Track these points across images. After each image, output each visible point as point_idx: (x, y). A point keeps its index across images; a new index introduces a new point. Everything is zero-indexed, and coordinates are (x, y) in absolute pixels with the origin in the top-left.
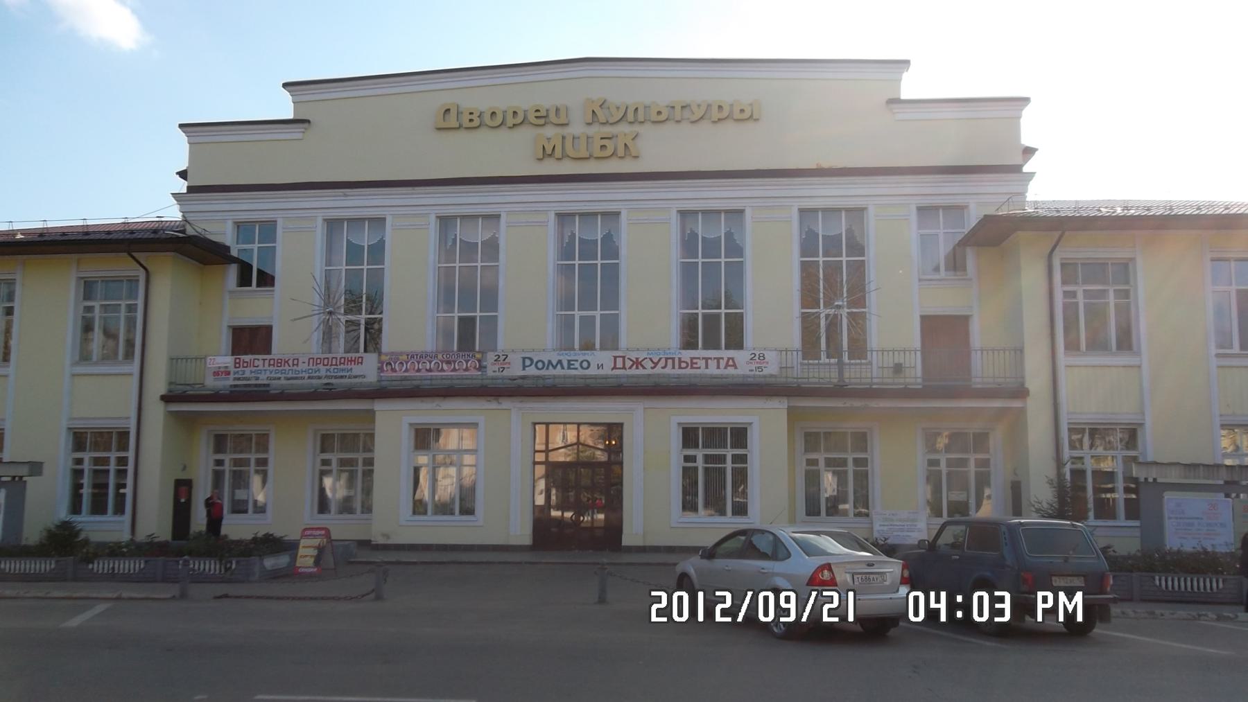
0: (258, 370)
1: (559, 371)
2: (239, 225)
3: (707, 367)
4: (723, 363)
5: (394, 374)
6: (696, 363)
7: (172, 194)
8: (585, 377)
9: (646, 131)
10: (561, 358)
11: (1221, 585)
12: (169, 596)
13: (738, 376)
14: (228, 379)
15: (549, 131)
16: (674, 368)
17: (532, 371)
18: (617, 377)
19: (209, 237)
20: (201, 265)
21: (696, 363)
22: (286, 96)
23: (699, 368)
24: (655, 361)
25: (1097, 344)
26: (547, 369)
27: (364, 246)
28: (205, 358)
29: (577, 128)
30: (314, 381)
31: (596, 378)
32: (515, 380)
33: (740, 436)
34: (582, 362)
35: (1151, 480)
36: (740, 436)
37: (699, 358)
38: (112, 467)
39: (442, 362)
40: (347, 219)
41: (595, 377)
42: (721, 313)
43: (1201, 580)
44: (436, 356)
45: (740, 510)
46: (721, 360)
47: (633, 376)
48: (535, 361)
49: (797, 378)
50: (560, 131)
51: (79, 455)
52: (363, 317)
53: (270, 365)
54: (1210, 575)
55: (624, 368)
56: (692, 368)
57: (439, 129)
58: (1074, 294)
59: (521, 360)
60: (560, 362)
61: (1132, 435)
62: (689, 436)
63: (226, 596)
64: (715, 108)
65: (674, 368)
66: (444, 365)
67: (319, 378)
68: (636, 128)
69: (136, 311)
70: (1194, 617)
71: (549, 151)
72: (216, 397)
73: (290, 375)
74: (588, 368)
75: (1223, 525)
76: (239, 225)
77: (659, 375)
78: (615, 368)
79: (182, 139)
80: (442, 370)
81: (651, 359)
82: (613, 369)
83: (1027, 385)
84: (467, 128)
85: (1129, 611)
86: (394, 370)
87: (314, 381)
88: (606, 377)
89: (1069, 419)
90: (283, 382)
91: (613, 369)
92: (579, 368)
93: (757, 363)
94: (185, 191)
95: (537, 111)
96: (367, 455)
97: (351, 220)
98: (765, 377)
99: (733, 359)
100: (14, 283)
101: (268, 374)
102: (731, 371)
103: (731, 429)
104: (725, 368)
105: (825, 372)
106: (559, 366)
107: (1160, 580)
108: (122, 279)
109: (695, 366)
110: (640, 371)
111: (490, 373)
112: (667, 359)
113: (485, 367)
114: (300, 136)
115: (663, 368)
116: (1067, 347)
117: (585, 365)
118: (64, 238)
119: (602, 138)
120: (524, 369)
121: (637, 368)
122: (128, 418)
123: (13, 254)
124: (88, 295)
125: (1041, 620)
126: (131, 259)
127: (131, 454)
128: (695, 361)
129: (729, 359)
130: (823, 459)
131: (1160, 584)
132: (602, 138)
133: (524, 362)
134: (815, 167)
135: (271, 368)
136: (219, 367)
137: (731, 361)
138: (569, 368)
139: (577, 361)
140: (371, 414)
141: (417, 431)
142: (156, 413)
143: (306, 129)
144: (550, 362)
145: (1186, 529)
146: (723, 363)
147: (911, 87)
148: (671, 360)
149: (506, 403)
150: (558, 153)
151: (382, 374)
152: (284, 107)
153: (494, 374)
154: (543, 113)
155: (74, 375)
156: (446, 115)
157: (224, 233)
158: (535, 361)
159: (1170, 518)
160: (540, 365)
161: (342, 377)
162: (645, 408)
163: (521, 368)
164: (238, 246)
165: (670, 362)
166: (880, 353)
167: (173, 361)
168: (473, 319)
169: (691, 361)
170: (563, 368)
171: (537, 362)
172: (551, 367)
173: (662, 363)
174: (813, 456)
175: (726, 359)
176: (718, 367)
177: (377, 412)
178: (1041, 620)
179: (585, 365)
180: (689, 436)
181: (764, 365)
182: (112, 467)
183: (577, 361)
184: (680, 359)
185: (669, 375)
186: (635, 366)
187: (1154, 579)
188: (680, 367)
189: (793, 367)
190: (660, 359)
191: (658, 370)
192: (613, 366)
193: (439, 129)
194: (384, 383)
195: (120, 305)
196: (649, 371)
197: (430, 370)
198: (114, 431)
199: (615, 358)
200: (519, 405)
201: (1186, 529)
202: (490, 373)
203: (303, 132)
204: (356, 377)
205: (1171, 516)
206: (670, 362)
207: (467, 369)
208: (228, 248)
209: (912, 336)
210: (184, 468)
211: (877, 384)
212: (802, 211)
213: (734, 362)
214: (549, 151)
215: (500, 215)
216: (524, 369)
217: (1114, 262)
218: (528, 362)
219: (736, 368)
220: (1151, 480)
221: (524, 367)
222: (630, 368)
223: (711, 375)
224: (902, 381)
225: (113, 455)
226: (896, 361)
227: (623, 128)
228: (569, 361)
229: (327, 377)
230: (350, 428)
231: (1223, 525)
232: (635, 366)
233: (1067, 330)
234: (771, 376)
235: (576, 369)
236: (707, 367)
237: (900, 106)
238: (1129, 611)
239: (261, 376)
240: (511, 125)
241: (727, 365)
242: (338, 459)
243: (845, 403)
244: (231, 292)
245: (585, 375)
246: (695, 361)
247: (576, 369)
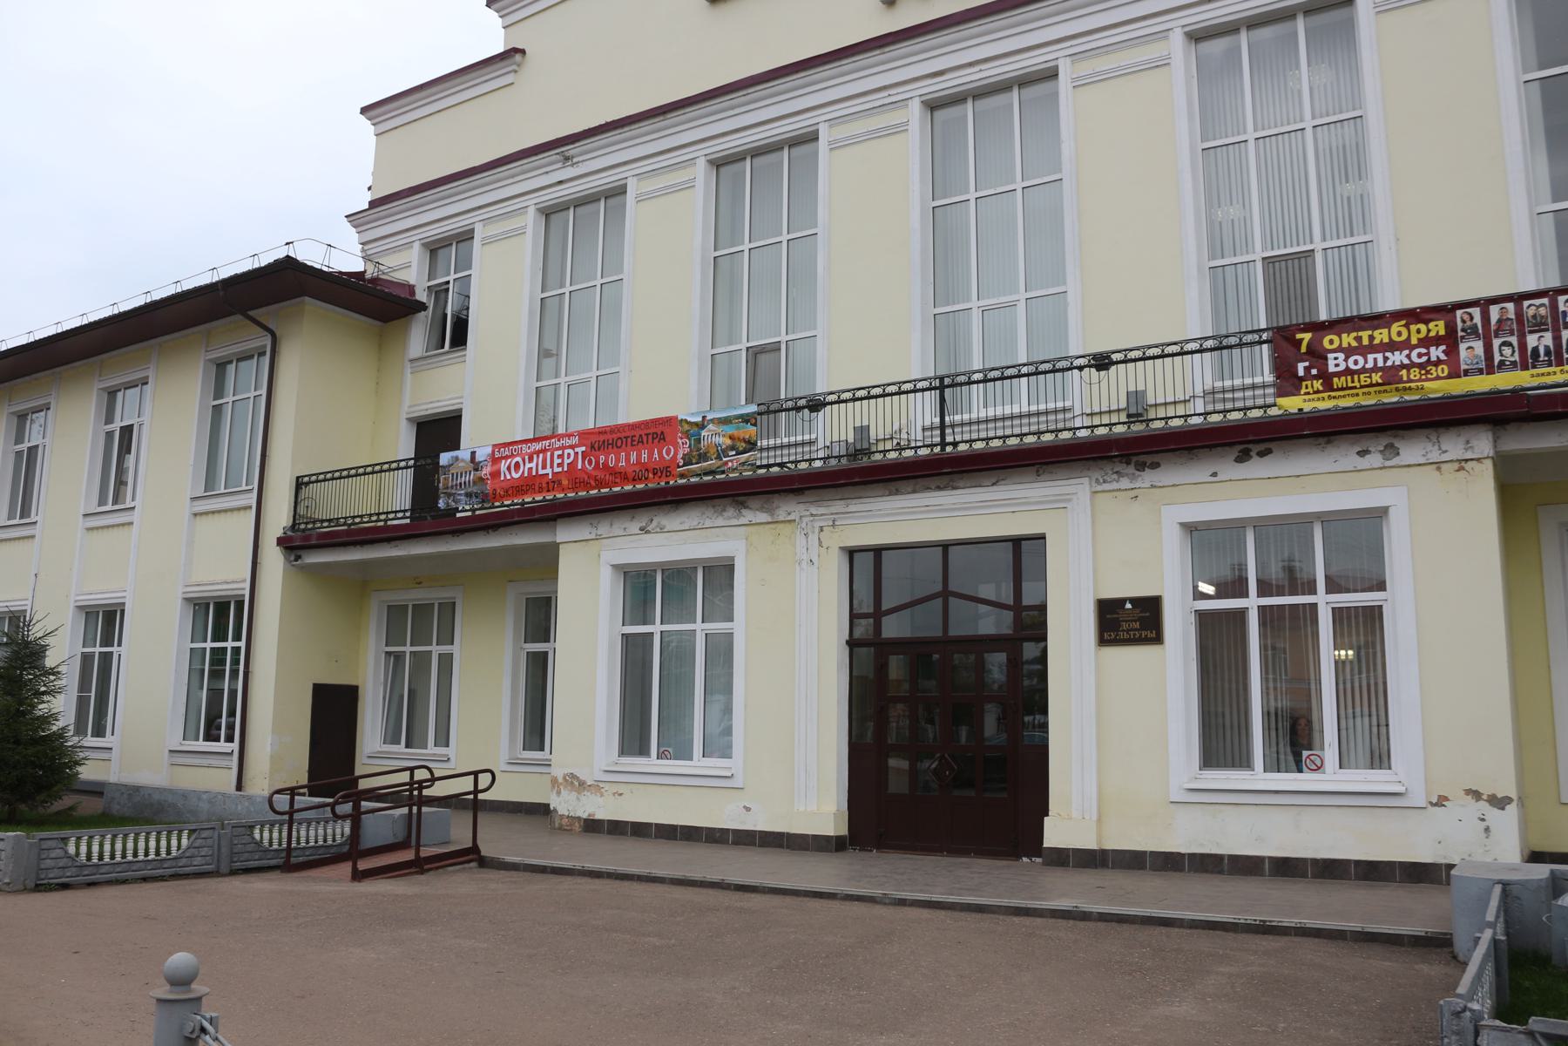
2: (434, 249)
79: (366, 126)
105: (768, 457)
116: (242, 602)
125: (1367, 343)
126: (249, 322)
127: (242, 644)
131: (78, 854)
142: (274, 558)
178: (1367, 343)
203: (516, 71)
231: (1034, 719)
233: (237, 671)
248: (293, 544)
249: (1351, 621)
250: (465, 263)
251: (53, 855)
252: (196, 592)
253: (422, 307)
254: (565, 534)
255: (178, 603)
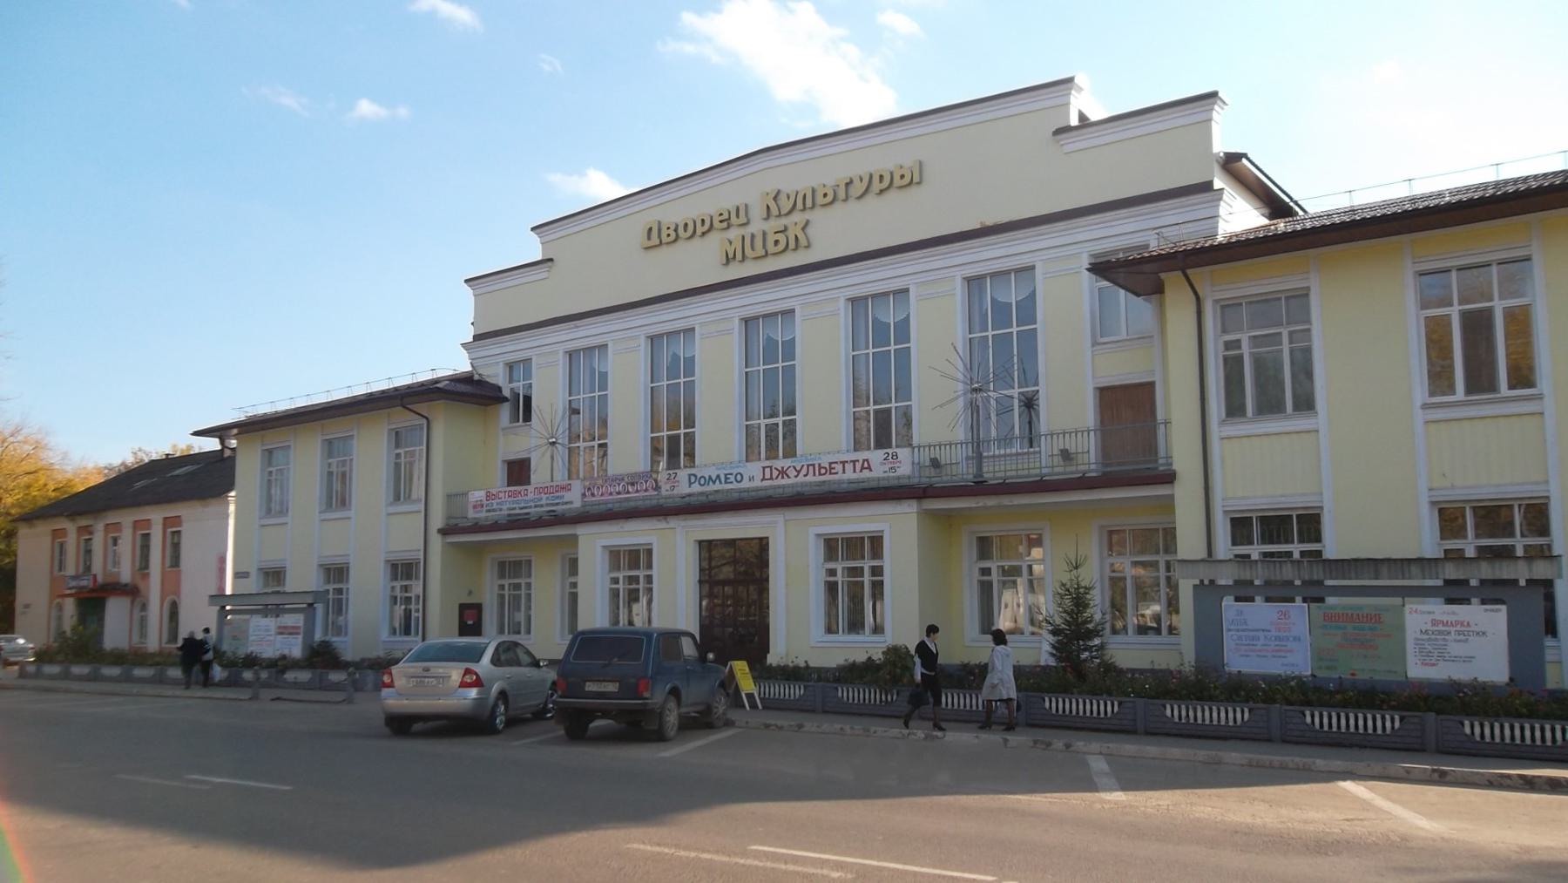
0: (529, 499)
1: (717, 486)
2: (511, 366)
3: (844, 472)
4: (858, 466)
5: (594, 499)
6: (834, 468)
7: (462, 344)
8: (740, 491)
9: (818, 217)
10: (719, 472)
11: (1397, 725)
12: (341, 699)
13: (873, 479)
14: (482, 511)
15: (734, 234)
16: (814, 474)
17: (696, 488)
18: (766, 488)
19: (488, 380)
20: (482, 407)
21: (834, 468)
22: (535, 239)
23: (836, 473)
24: (798, 468)
25: (1270, 405)
26: (708, 484)
27: (889, 324)
28: (466, 494)
29: (757, 226)
30: (538, 509)
31: (748, 492)
32: (684, 497)
33: (876, 542)
34: (736, 475)
35: (1206, 582)
36: (876, 542)
37: (836, 463)
38: (867, 579)
39: (628, 484)
40: (583, 349)
41: (748, 490)
42: (891, 408)
43: (1067, 701)
44: (623, 479)
45: (878, 629)
46: (857, 463)
47: (779, 487)
48: (699, 477)
49: (930, 477)
50: (741, 231)
51: (831, 565)
52: (780, 420)
53: (509, 496)
54: (1105, 696)
55: (771, 478)
56: (831, 473)
57: (646, 248)
58: (1236, 344)
59: (687, 477)
60: (718, 476)
61: (1310, 524)
62: (831, 546)
63: (278, 699)
64: (876, 179)
65: (814, 474)
66: (630, 487)
67: (542, 506)
68: (808, 215)
69: (400, 458)
70: (903, 735)
71: (731, 256)
72: (495, 527)
73: (522, 505)
74: (741, 481)
75: (1297, 639)
76: (511, 366)
77: (802, 483)
78: (763, 479)
79: (468, 292)
80: (628, 492)
81: (794, 468)
82: (762, 480)
83: (1175, 467)
84: (668, 243)
85: (847, 728)
86: (593, 495)
87: (538, 509)
88: (757, 489)
89: (1223, 506)
90: (518, 511)
91: (762, 480)
92: (735, 482)
93: (891, 462)
94: (472, 340)
95: (721, 214)
96: (876, 563)
97: (994, 275)
98: (899, 478)
99: (867, 460)
100: (1307, 295)
101: (508, 506)
102: (866, 474)
103: (1298, 516)
104: (861, 471)
106: (718, 481)
107: (1313, 716)
108: (1279, 296)
109: (833, 471)
110: (785, 481)
111: (664, 493)
112: (808, 466)
113: (660, 488)
114: (544, 275)
115: (805, 476)
117: (739, 478)
118: (397, 393)
119: (776, 233)
120: (690, 486)
121: (783, 477)
122: (419, 550)
123: (453, 400)
124: (330, 455)
128: (833, 466)
129: (864, 461)
130: (1522, 547)
131: (1050, 707)
132: (776, 233)
133: (690, 480)
134: (979, 227)
135: (510, 499)
136: (477, 501)
137: (866, 463)
138: (726, 482)
139: (731, 474)
140: (575, 537)
141: (1233, 520)
142: (436, 542)
143: (550, 267)
144: (710, 478)
145: (1249, 645)
146: (858, 466)
147: (1090, 102)
148: (769, 469)
149: (674, 522)
150: (739, 256)
151: (585, 500)
152: (533, 250)
153: (667, 493)
154: (726, 216)
155: (389, 514)
156: (778, 202)
157: (496, 374)
158: (699, 477)
159: (1229, 630)
160: (702, 481)
161: (557, 504)
162: (786, 521)
163: (688, 485)
164: (1098, 284)
165: (811, 468)
166: (1049, 437)
167: (450, 497)
168: (888, 411)
169: (830, 466)
170: (720, 482)
171: (700, 478)
172: (711, 483)
173: (804, 471)
174: (986, 564)
175: (861, 462)
176: (855, 471)
177: (580, 538)
179: (739, 478)
180: (831, 546)
181: (898, 464)
182: (867, 579)
183: (731, 474)
184: (819, 465)
185: (810, 483)
186: (780, 477)
187: (1305, 716)
188: (820, 474)
189: (1088, 451)
190: (803, 466)
191: (801, 478)
192: (762, 477)
193: (646, 248)
194: (588, 508)
195: (1280, 334)
196: (792, 481)
197: (619, 493)
198: (641, 548)
199: (764, 468)
200: (683, 523)
201: (1249, 645)
202: (664, 493)
204: (566, 503)
205: (1232, 627)
206: (811, 468)
207: (646, 490)
208: (499, 389)
209: (1088, 415)
210: (470, 593)
211: (1012, 478)
212: (969, 280)
213: (868, 463)
214: (731, 256)
215: (794, 309)
216: (690, 486)
217: (1289, 294)
218: (693, 479)
219: (871, 470)
220: (1206, 582)
221: (690, 484)
222: (777, 477)
223: (848, 480)
224: (1073, 468)
225: (867, 564)
226: (932, 456)
227: (798, 217)
228: (726, 475)
229: (547, 505)
230: (1144, 520)
231: (1297, 639)
232: (780, 477)
234: (904, 477)
235: (732, 482)
236: (844, 472)
237: (1090, 129)
238: (847, 728)
239: (504, 507)
240: (878, 192)
241: (863, 468)
242: (870, 566)
243: (978, 503)
244: (503, 429)
245: (740, 489)
246: (833, 466)
247: (732, 482)
248: (444, 532)
249: (419, 601)
250: (528, 374)
251: (1294, 721)
252: (264, 565)
253: (505, 399)
254: (582, 531)
255: (382, 564)
